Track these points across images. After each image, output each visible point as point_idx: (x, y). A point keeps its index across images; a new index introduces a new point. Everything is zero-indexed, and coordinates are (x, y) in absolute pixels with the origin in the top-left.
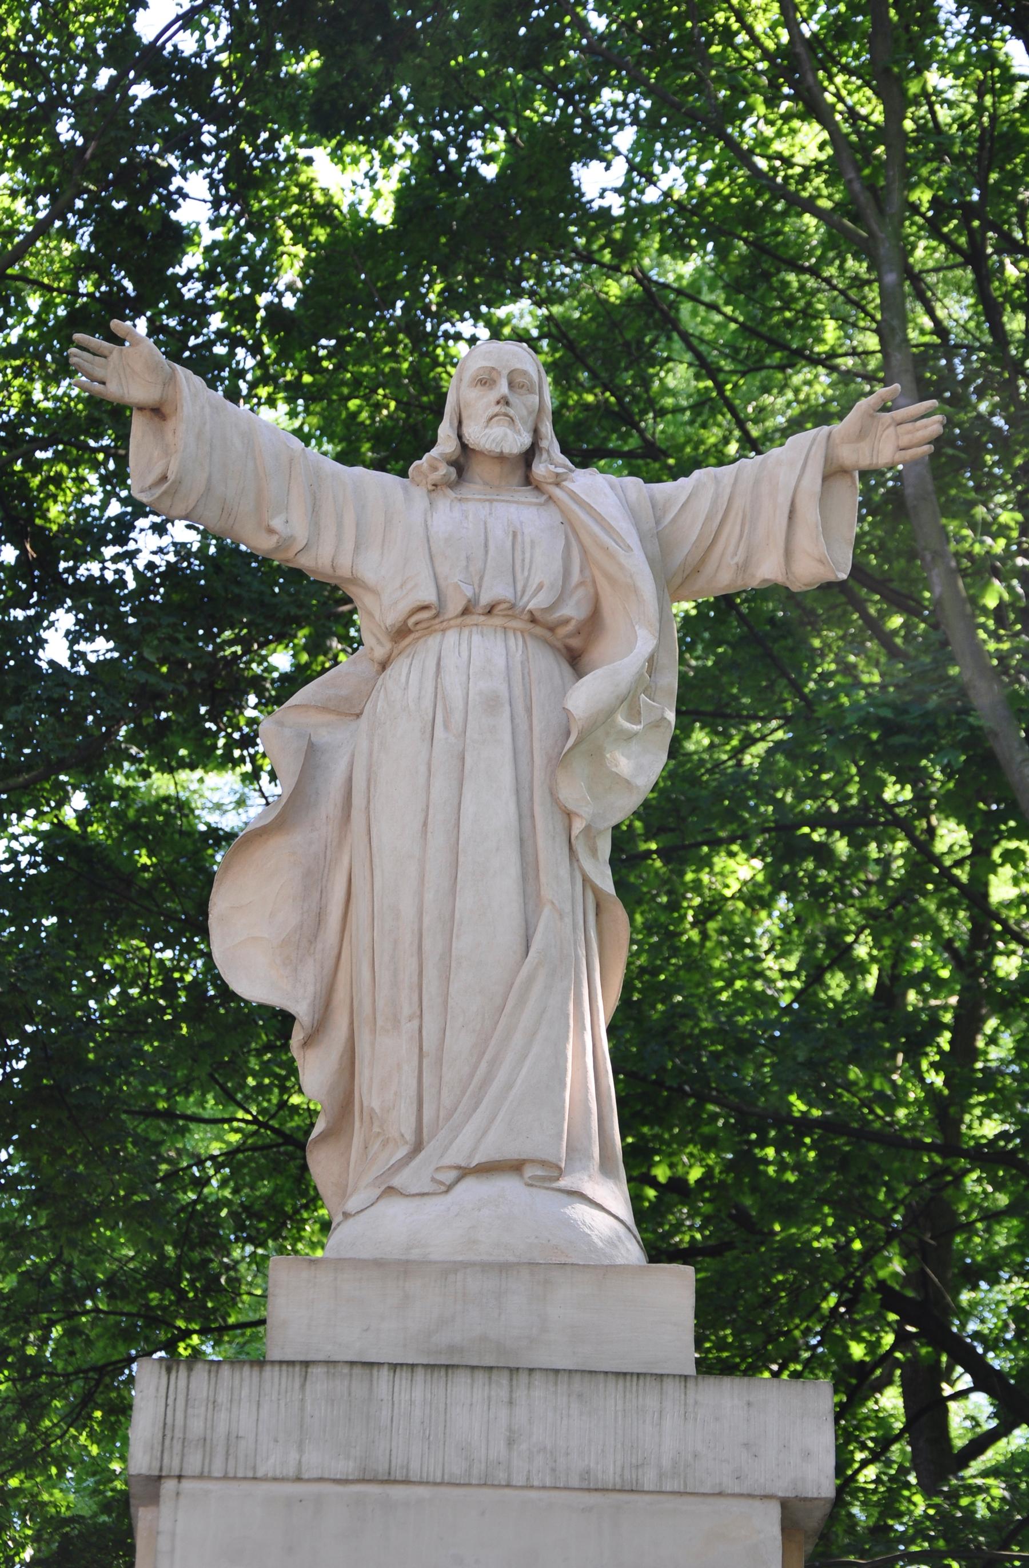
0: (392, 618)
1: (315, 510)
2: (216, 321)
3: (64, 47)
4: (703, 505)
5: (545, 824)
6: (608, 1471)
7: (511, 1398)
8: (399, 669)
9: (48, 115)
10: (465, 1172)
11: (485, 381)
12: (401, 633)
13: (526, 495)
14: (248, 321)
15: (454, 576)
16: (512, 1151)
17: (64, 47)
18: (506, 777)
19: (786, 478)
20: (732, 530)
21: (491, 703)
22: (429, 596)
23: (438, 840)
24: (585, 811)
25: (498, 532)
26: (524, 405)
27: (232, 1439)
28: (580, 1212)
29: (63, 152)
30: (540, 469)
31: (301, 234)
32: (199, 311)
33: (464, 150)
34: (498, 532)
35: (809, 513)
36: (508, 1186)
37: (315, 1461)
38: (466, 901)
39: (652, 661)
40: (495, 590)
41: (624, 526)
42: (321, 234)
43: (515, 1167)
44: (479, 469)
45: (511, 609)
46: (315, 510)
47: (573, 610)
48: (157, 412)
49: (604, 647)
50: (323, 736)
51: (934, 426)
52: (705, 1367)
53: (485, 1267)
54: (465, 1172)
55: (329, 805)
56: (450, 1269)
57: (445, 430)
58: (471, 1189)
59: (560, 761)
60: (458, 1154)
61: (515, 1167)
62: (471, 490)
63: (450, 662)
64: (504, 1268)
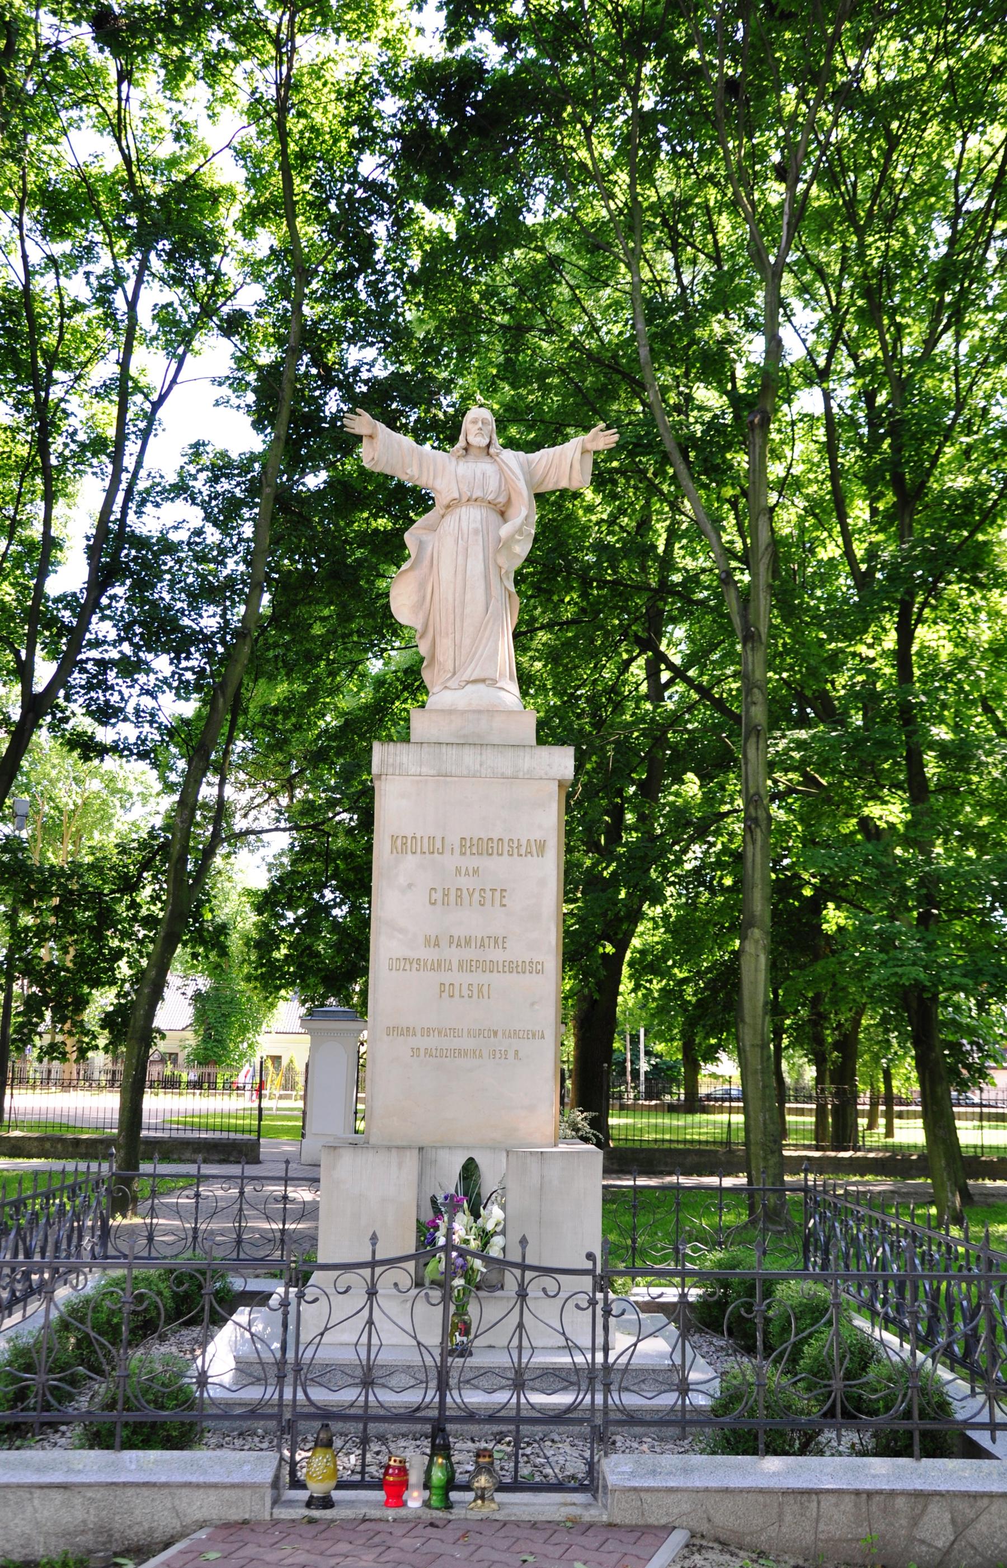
0: (445, 502)
1: (421, 466)
2: (389, 278)
3: (332, 175)
4: (543, 463)
5: (492, 571)
6: (509, 772)
7: (374, 1244)
8: (448, 518)
9: (326, 201)
10: (468, 682)
11: (474, 422)
12: (448, 507)
13: (488, 459)
14: (400, 277)
15: (464, 488)
16: (482, 676)
17: (332, 175)
18: (481, 557)
19: (570, 454)
20: (553, 470)
21: (476, 532)
22: (456, 495)
23: (460, 577)
24: (505, 567)
25: (479, 474)
26: (485, 431)
27: (401, 764)
28: (502, 693)
29: (333, 217)
30: (492, 450)
31: (421, 247)
32: (384, 274)
33: (482, 204)
34: (479, 474)
35: (577, 466)
36: (481, 687)
37: (425, 770)
38: (468, 596)
39: (527, 518)
40: (477, 493)
41: (518, 472)
42: (428, 247)
43: (483, 681)
44: (472, 451)
45: (483, 500)
46: (421, 466)
47: (502, 499)
48: (371, 437)
49: (511, 512)
50: (424, 538)
51: (616, 437)
52: (541, 741)
53: (474, 711)
54: (468, 682)
55: (426, 562)
56: (464, 712)
57: (462, 437)
58: (470, 688)
59: (497, 551)
60: (465, 677)
61: (483, 681)
62: (470, 458)
63: (464, 518)
64: (479, 712)
